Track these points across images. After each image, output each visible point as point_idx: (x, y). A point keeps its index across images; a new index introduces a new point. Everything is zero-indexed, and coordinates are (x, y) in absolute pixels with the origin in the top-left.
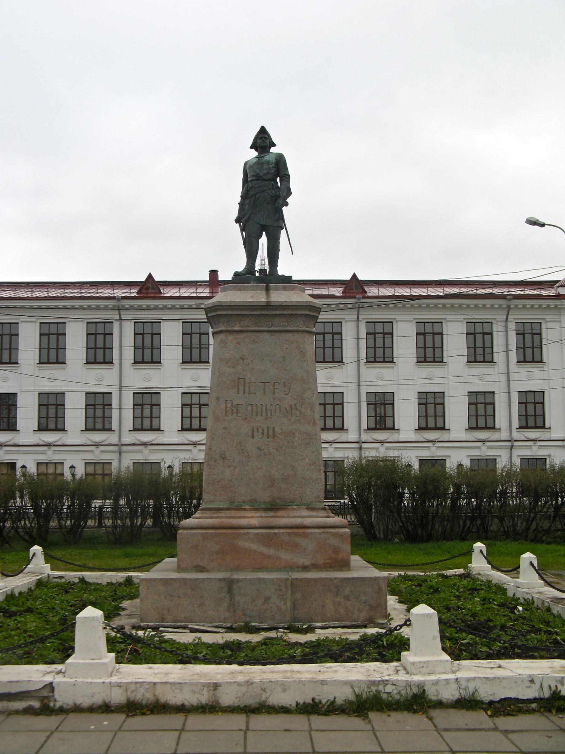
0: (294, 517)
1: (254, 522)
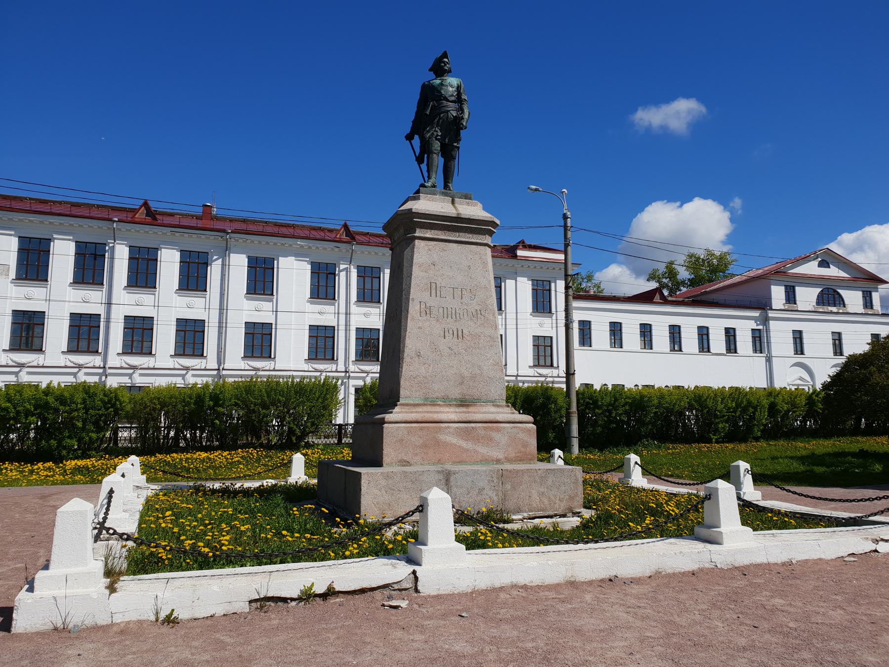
0: (484, 413)
1: (453, 417)
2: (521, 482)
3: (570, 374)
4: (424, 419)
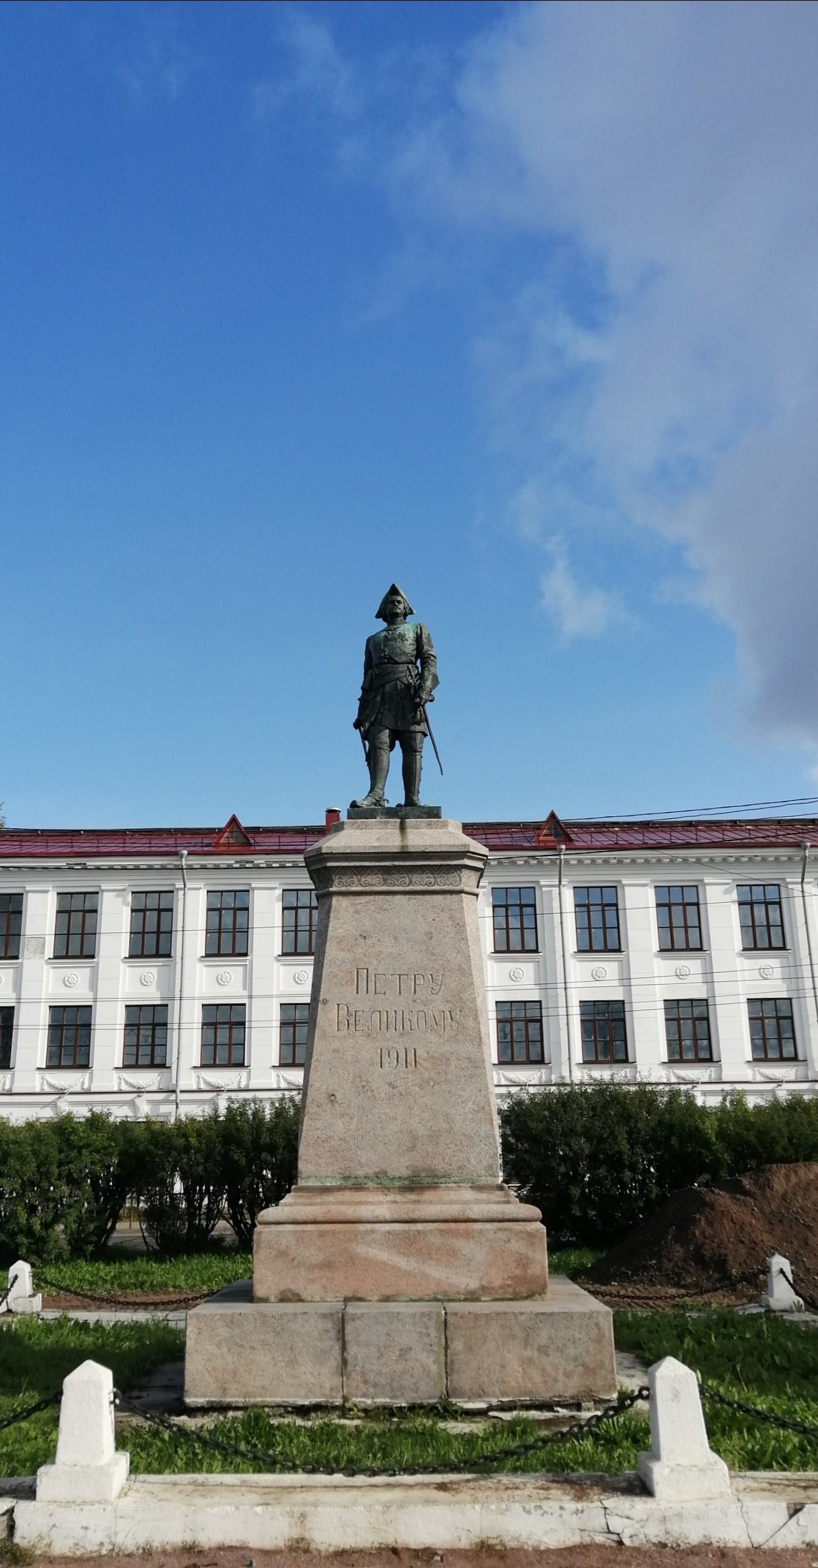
1: (383, 1211)
2: (485, 1338)
4: (329, 1217)
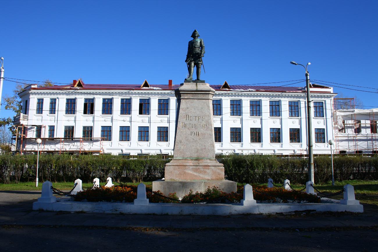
1: (191, 164)
3: (100, 138)
